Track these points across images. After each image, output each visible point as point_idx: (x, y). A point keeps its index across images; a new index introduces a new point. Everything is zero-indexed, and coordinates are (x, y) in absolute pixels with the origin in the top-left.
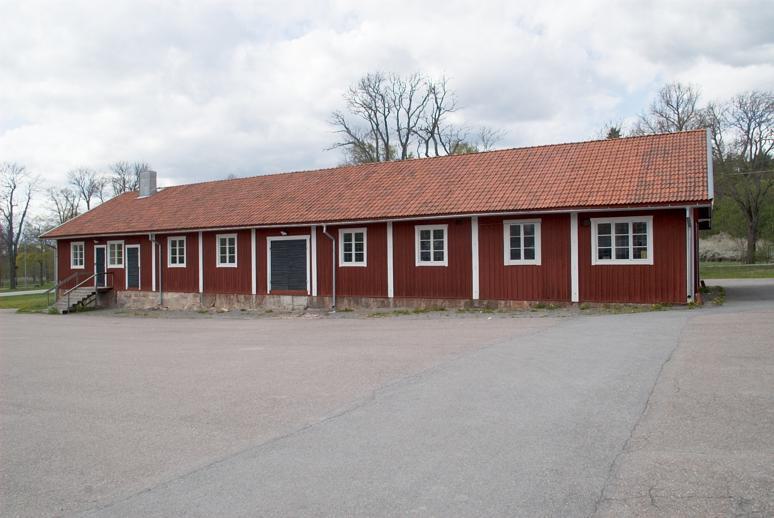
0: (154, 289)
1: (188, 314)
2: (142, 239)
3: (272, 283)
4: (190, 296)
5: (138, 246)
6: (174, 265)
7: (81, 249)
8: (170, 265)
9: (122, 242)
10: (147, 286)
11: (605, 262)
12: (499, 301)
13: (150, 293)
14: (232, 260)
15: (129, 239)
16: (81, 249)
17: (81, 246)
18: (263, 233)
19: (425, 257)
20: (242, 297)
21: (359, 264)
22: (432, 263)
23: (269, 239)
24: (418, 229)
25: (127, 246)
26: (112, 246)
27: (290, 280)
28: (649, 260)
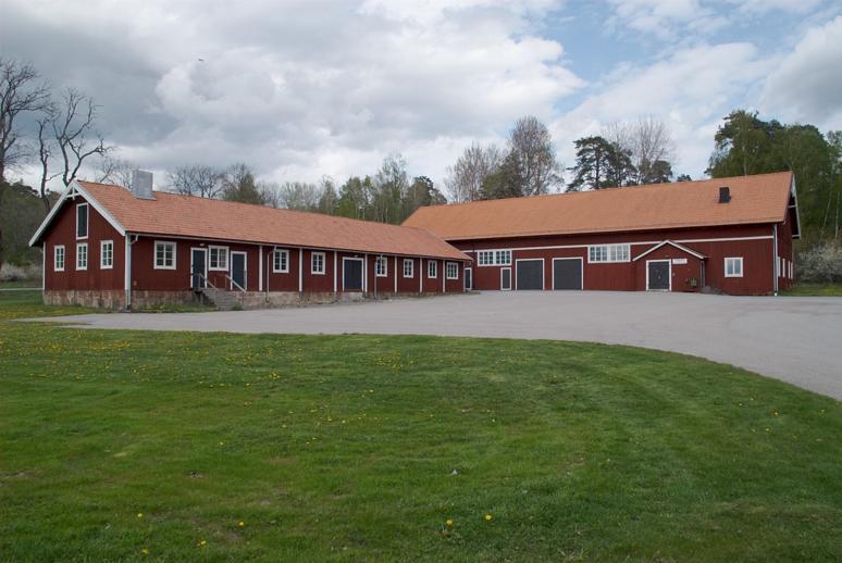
0: (261, 289)
1: (291, 306)
2: (252, 248)
3: (133, 278)
4: (291, 294)
5: (245, 253)
6: (730, 276)
7: (110, 248)
8: (275, 271)
9: (227, 248)
10: (253, 286)
11: (160, 267)
12: (68, 293)
13: (256, 293)
14: (320, 270)
15: (234, 245)
16: (110, 248)
17: (110, 245)
18: (342, 253)
19: (160, 263)
20: (327, 294)
21: (738, 275)
22: (164, 267)
23: (344, 258)
24: (156, 243)
25: (232, 252)
26: (214, 251)
27: (353, 284)
28: (173, 267)
